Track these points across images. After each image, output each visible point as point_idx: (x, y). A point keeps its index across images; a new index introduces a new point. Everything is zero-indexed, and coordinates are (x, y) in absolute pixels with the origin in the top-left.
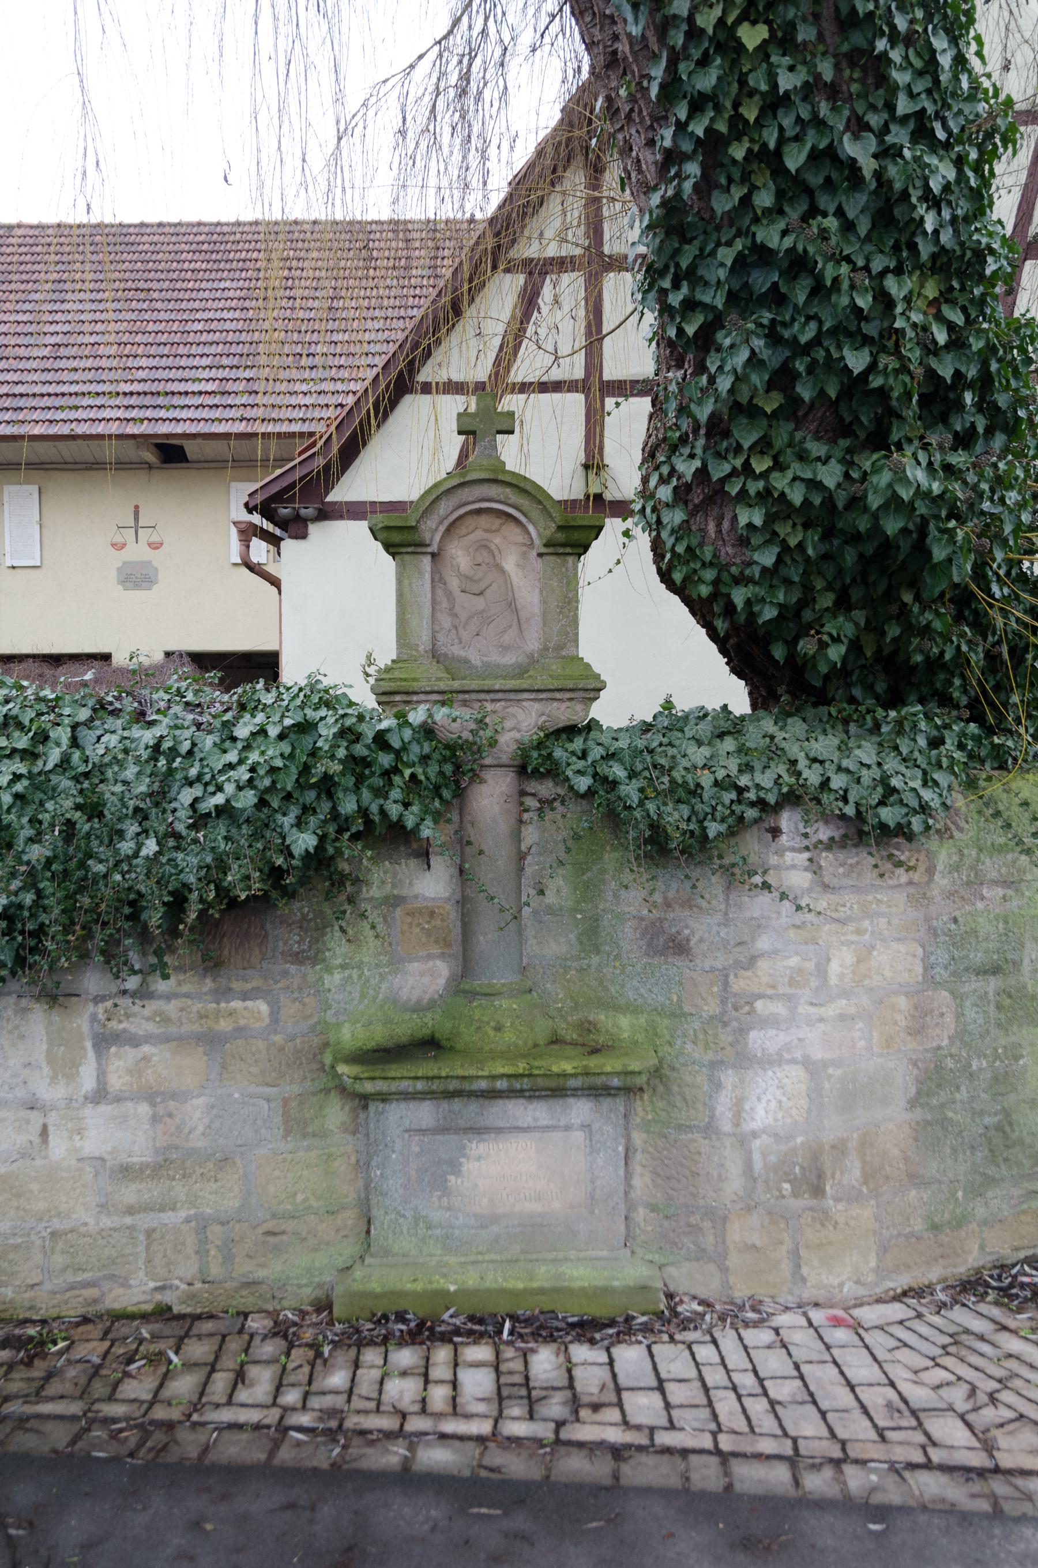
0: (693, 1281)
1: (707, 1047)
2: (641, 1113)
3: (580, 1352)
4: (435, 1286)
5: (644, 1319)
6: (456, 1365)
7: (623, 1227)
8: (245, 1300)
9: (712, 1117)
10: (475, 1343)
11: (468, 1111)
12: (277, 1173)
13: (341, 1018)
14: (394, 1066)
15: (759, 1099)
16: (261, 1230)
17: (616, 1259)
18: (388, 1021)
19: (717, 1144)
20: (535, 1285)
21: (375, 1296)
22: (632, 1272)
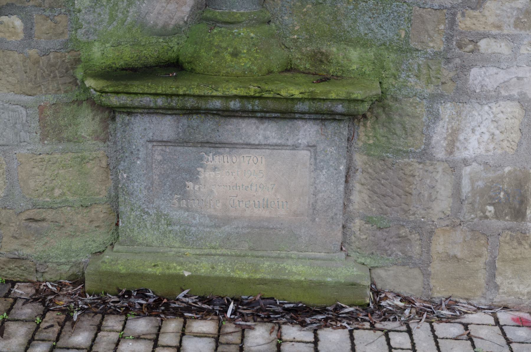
0: (397, 281)
1: (429, 81)
2: (363, 138)
3: (291, 332)
4: (172, 271)
5: (352, 309)
6: (183, 334)
7: (340, 234)
8: (13, 271)
9: (428, 145)
10: (202, 318)
11: (206, 127)
12: (36, 170)
13: (92, 38)
14: (136, 83)
15: (473, 131)
16: (24, 216)
17: (331, 260)
18: (135, 43)
19: (431, 168)
20: (258, 276)
21: (122, 276)
22: (344, 271)
